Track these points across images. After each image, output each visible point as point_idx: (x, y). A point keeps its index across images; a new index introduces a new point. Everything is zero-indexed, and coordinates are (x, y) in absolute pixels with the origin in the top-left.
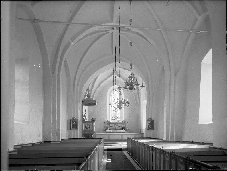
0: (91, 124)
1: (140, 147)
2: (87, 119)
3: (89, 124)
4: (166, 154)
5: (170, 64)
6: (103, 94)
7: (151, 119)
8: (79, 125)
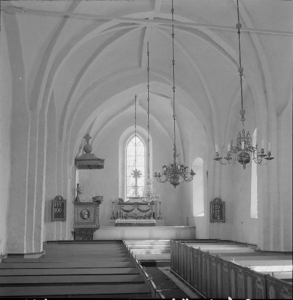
1: (191, 255)
2: (83, 198)
3: (88, 209)
4: (256, 278)
5: (265, 92)
6: (115, 141)
7: (220, 200)
8: (70, 209)
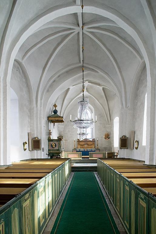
0: (56, 143)
8: (44, 144)
